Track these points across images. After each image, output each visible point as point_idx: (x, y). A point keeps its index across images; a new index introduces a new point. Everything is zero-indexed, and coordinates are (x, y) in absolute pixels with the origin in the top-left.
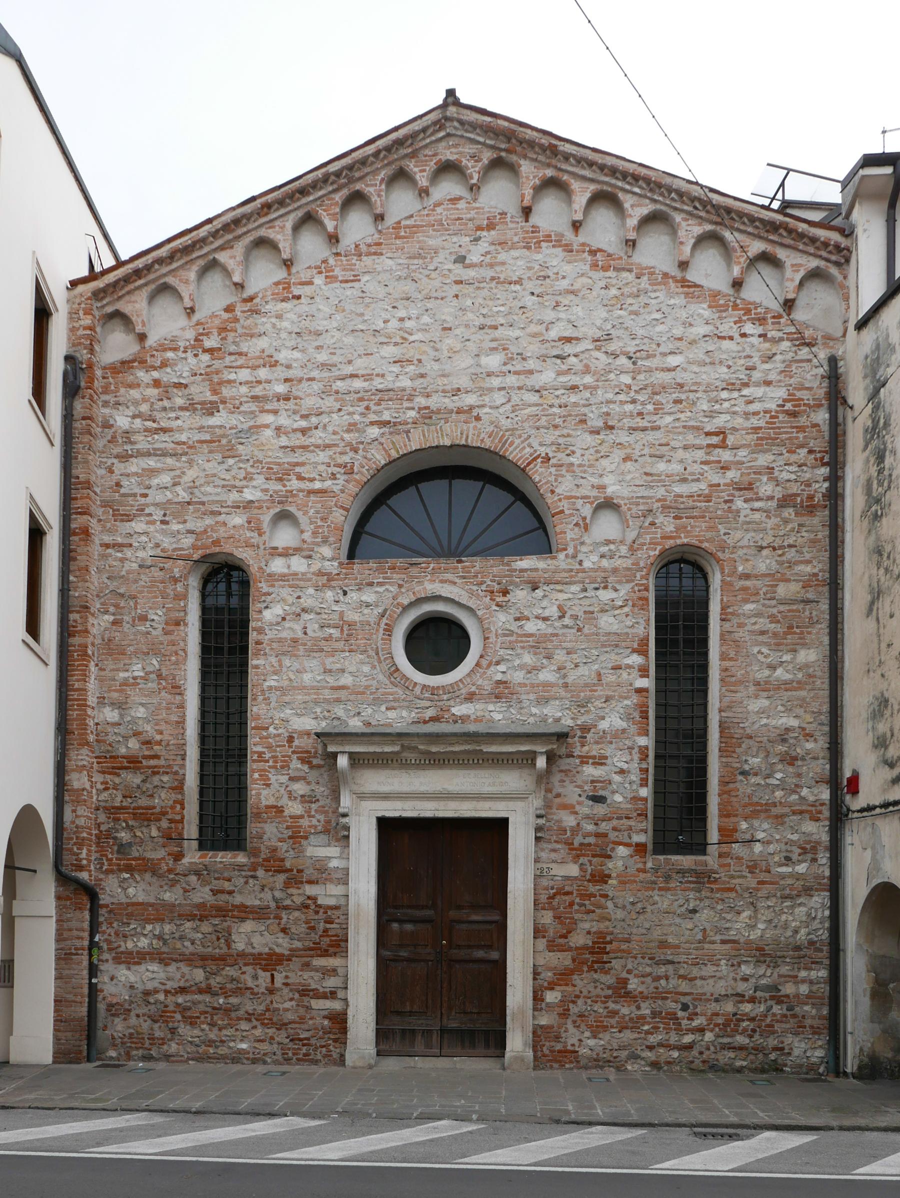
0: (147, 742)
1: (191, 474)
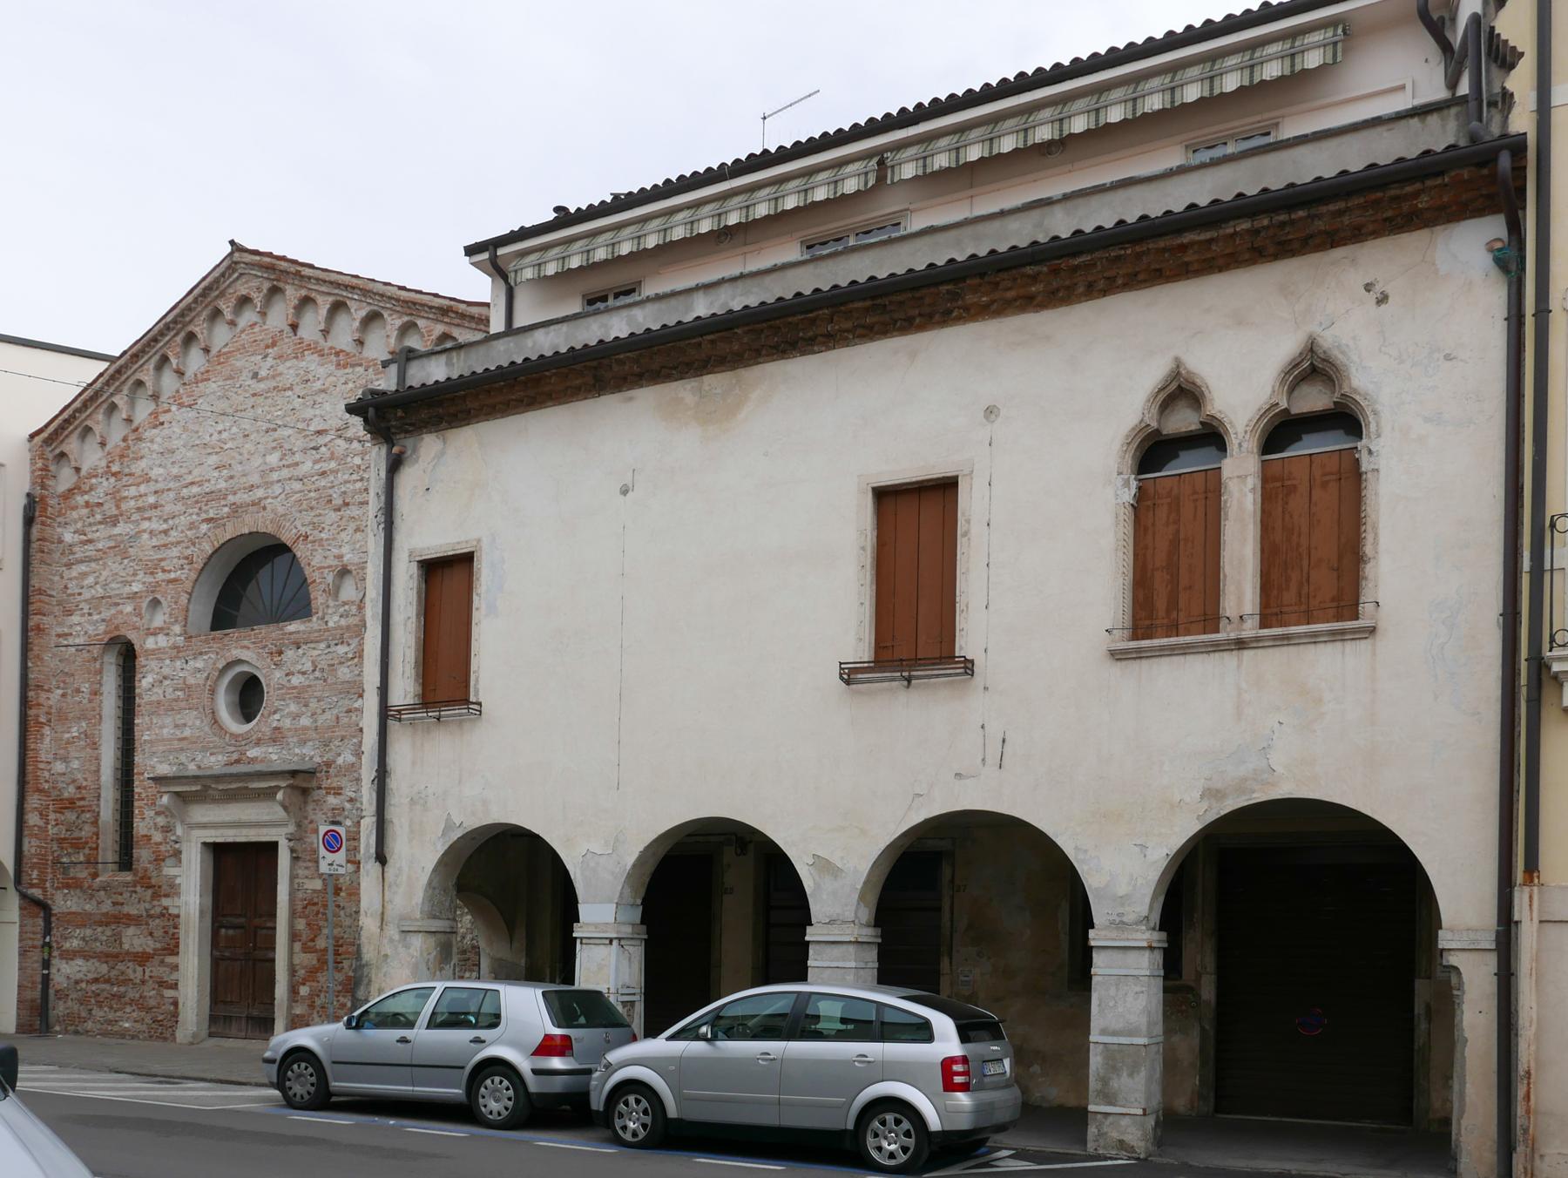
0: (79, 788)
1: (105, 573)
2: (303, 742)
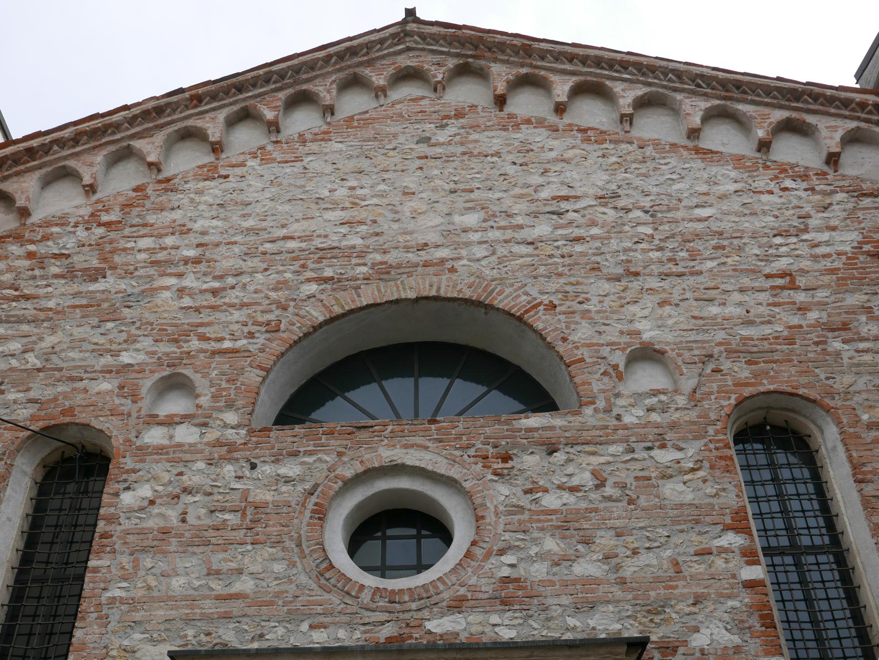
2: (838, 354)
